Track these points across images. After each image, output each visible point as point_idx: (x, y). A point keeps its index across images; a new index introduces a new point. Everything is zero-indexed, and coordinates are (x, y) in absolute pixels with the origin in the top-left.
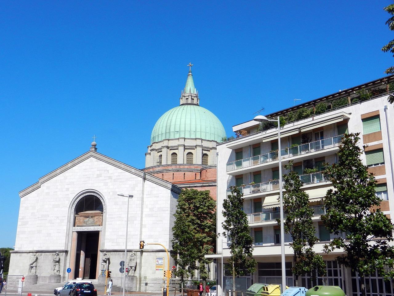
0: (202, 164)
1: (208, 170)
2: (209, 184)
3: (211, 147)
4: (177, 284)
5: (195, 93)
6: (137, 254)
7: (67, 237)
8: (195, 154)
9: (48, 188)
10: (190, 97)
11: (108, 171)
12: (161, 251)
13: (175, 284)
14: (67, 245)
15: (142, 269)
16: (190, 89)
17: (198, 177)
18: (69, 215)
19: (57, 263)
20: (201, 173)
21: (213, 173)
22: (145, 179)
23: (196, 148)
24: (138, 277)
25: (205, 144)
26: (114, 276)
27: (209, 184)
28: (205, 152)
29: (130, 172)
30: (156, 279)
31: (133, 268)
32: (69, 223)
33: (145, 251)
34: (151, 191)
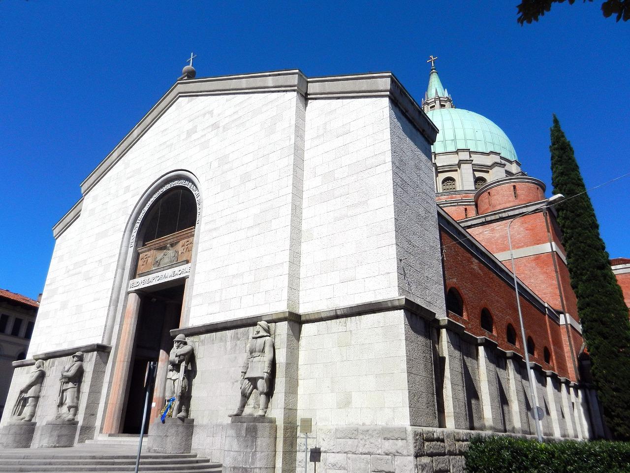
0: (476, 188)
1: (493, 191)
2: (500, 215)
3: (489, 164)
4: (451, 453)
5: (446, 94)
6: (278, 332)
7: (112, 308)
8: (460, 178)
9: (95, 198)
10: (438, 102)
11: (211, 113)
12: (367, 308)
13: (444, 454)
14: (109, 331)
15: (301, 390)
16: (436, 90)
17: (472, 213)
18: (123, 251)
19: (70, 385)
20: (476, 206)
21: (505, 193)
22: (305, 97)
23: (459, 167)
24: (280, 423)
25: (478, 160)
26: (205, 421)
27: (500, 215)
28: (478, 174)
29: (264, 90)
30: (353, 433)
31: (262, 385)
32: (120, 271)
33: (308, 318)
34: (325, 123)
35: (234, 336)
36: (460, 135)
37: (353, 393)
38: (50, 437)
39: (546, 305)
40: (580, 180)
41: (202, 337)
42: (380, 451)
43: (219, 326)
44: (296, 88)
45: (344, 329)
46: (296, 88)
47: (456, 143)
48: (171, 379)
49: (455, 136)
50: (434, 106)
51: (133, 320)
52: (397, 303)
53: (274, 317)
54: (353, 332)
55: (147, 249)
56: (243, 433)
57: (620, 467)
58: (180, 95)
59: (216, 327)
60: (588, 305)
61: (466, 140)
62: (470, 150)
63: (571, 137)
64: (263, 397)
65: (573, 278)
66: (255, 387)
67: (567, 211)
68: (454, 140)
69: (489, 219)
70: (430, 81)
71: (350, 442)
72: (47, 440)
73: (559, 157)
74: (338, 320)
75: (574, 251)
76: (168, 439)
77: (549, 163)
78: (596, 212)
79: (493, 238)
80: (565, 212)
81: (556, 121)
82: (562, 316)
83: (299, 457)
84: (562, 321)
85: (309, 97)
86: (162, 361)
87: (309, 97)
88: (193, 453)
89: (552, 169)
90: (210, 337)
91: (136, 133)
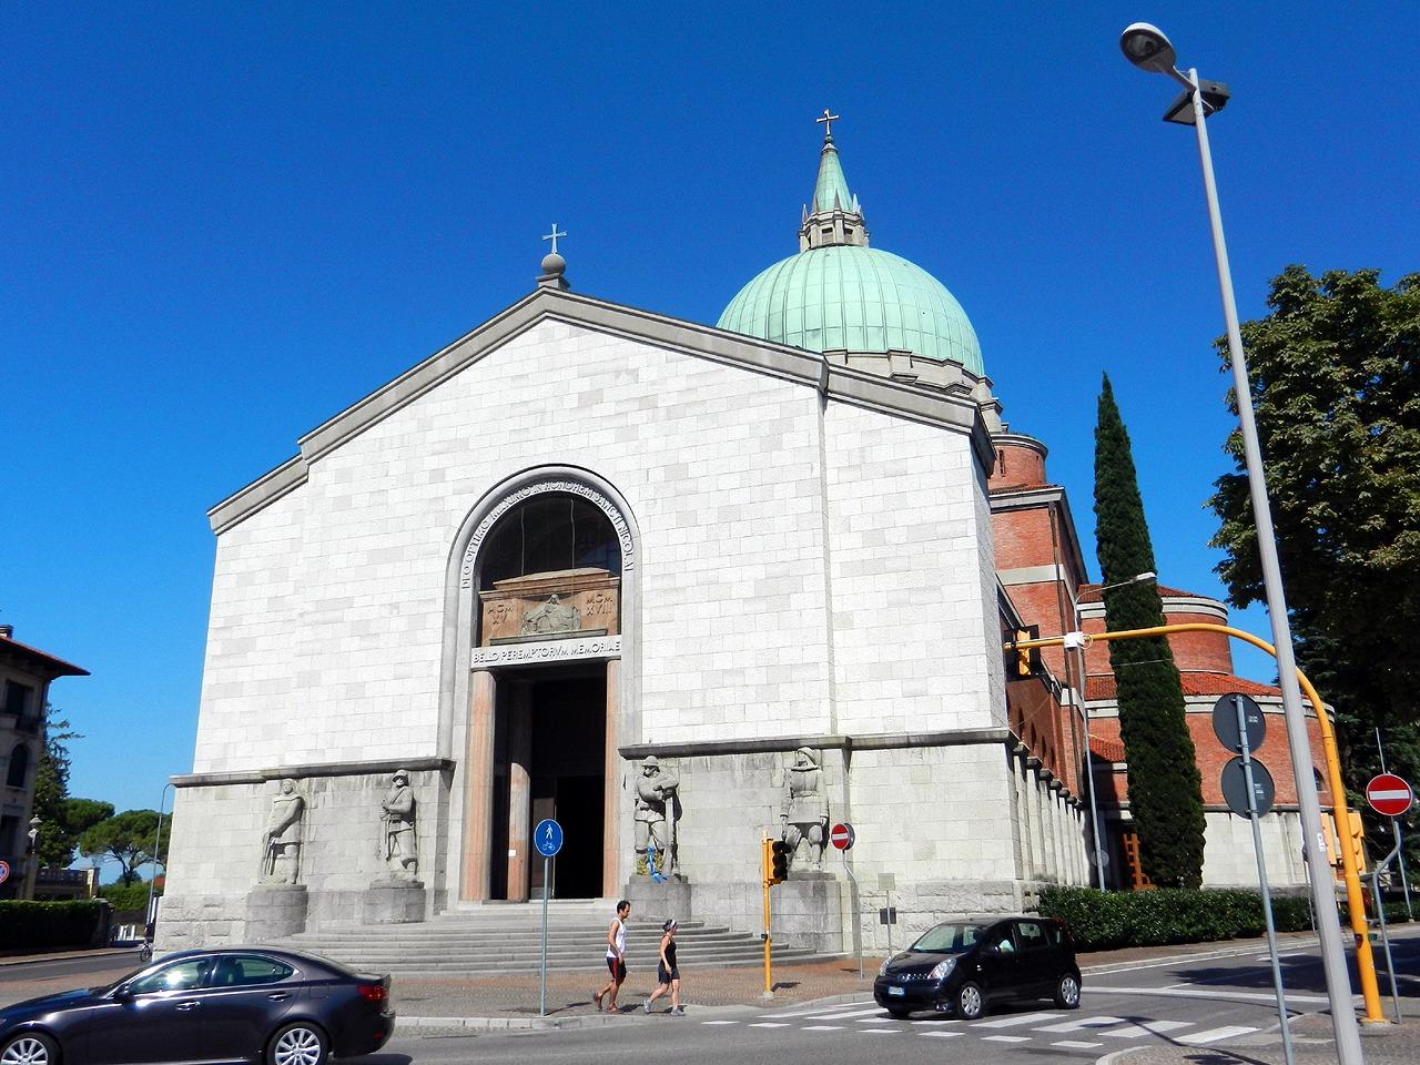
3: (943, 384)
5: (856, 208)
9: (344, 476)
11: (634, 373)
14: (445, 733)
32: (450, 630)
33: (863, 743)
35: (748, 763)
37: (937, 843)
38: (393, 907)
39: (1053, 679)
40: (1137, 495)
41: (685, 760)
42: (979, 909)
43: (719, 748)
44: (817, 383)
45: (920, 762)
46: (817, 383)
48: (645, 821)
49: (884, 318)
50: (831, 230)
51: (490, 717)
52: (997, 736)
53: (821, 742)
54: (933, 767)
55: (497, 595)
56: (811, 893)
57: (1177, 919)
58: (547, 314)
59: (714, 748)
60: (1134, 695)
63: (1128, 418)
64: (817, 847)
65: (1115, 652)
66: (805, 835)
67: (1115, 544)
68: (884, 328)
70: (822, 170)
71: (937, 899)
72: (390, 911)
74: (910, 750)
75: (1122, 612)
76: (669, 903)
77: (1090, 459)
78: (1154, 550)
80: (1112, 546)
81: (1107, 386)
82: (1065, 691)
83: (241, 942)
84: (1065, 700)
85: (829, 394)
86: (518, 782)
87: (829, 394)
88: (695, 921)
89: (1097, 469)
90: (701, 762)
91: (442, 364)
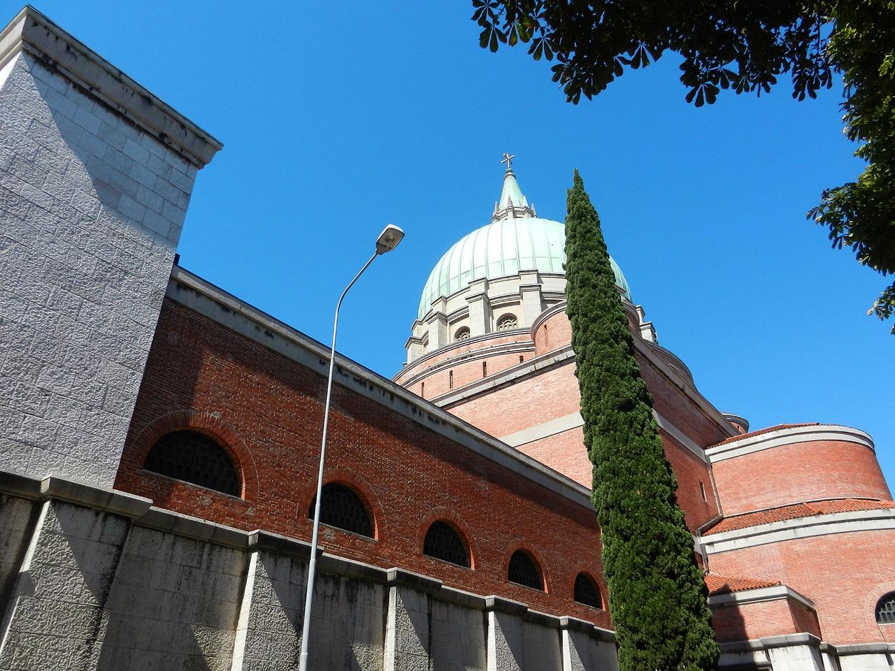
5: (525, 203)
36: (525, 251)
47: (519, 263)
61: (534, 258)
62: (540, 272)
68: (518, 259)
69: (540, 365)
73: (572, 231)
79: (547, 396)
81: (578, 179)
